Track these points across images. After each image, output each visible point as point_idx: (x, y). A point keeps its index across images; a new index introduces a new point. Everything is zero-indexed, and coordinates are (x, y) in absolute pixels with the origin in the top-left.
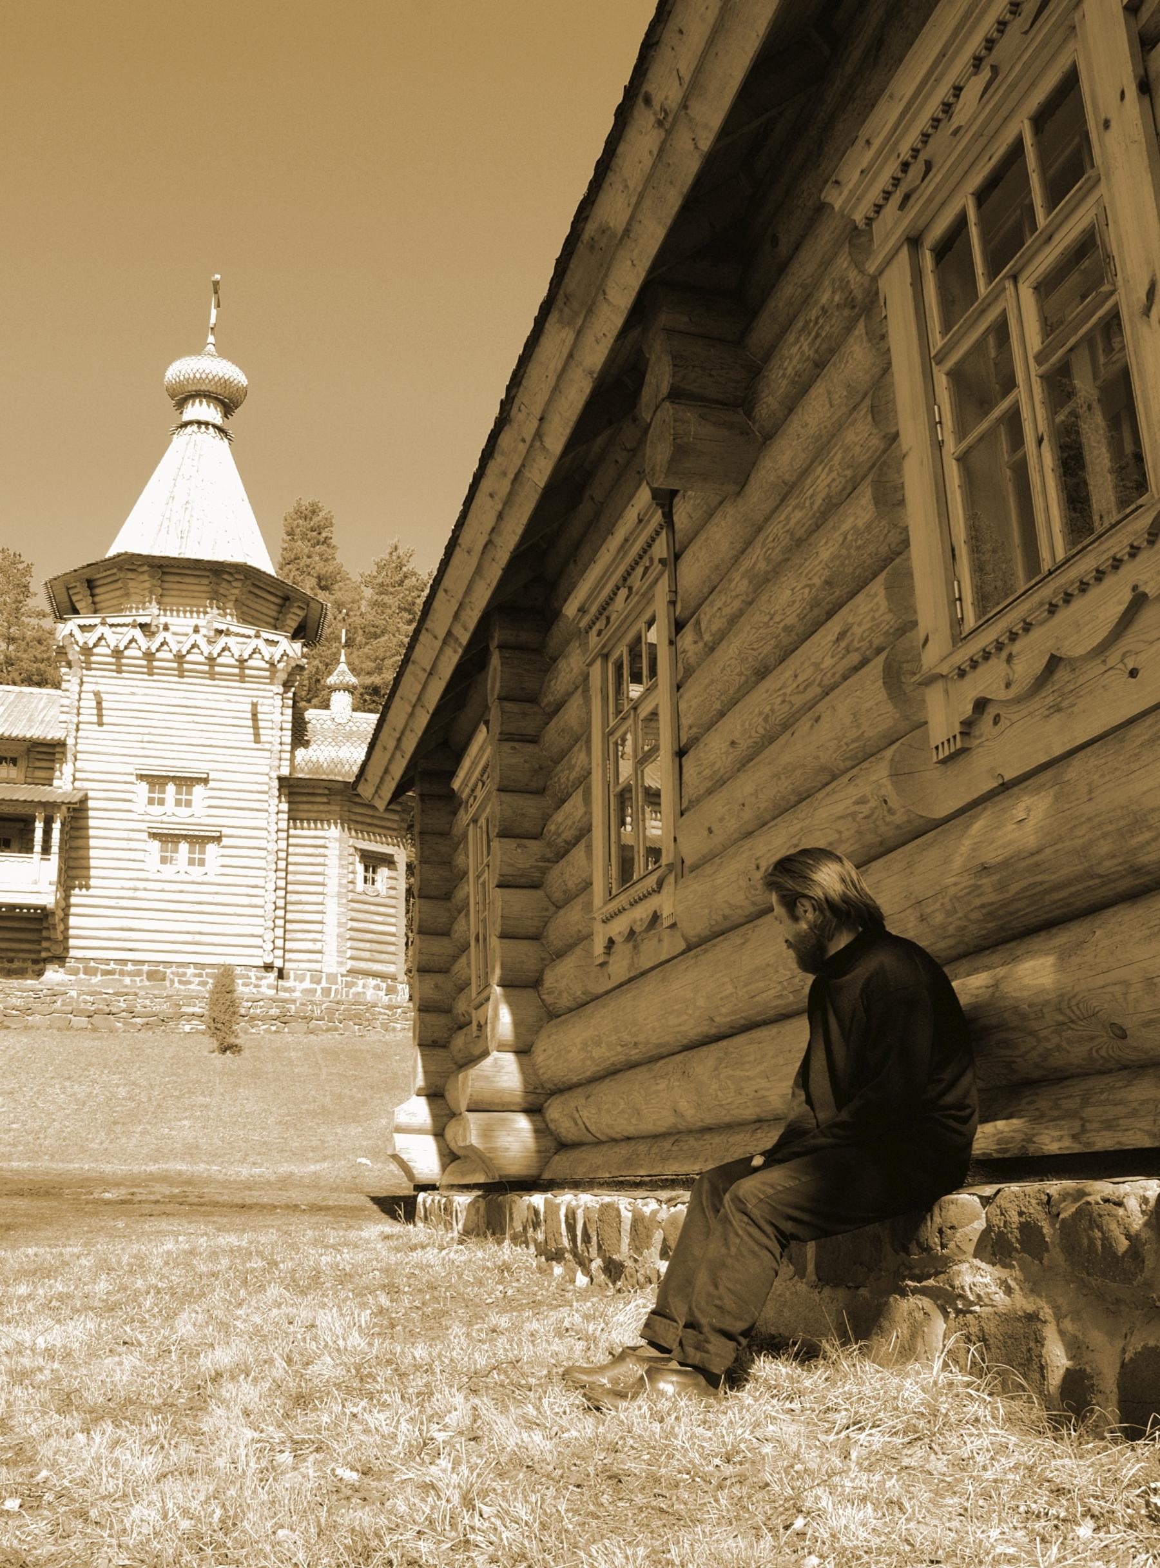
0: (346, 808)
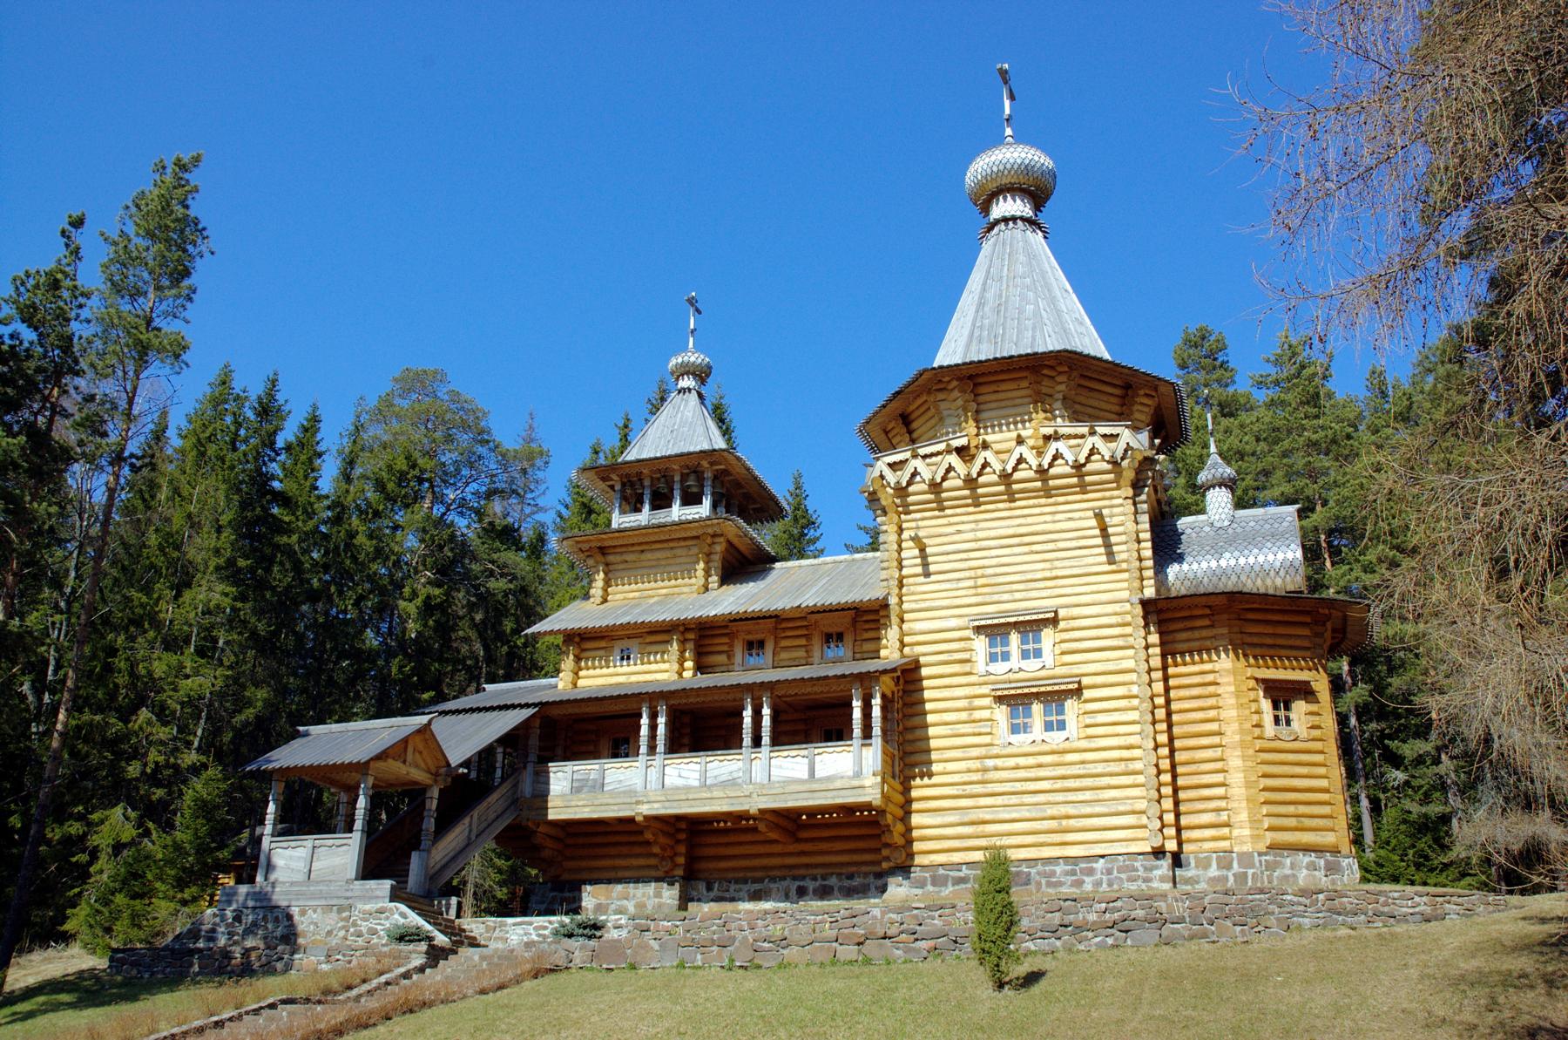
0: (1236, 629)
